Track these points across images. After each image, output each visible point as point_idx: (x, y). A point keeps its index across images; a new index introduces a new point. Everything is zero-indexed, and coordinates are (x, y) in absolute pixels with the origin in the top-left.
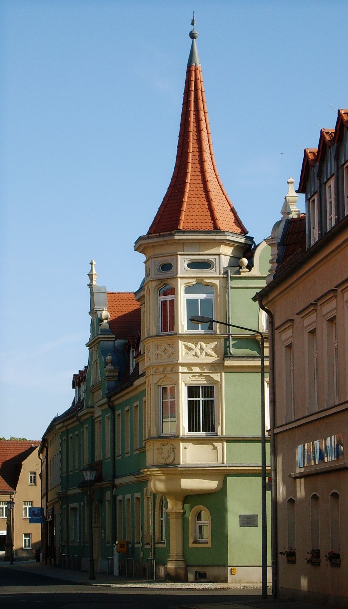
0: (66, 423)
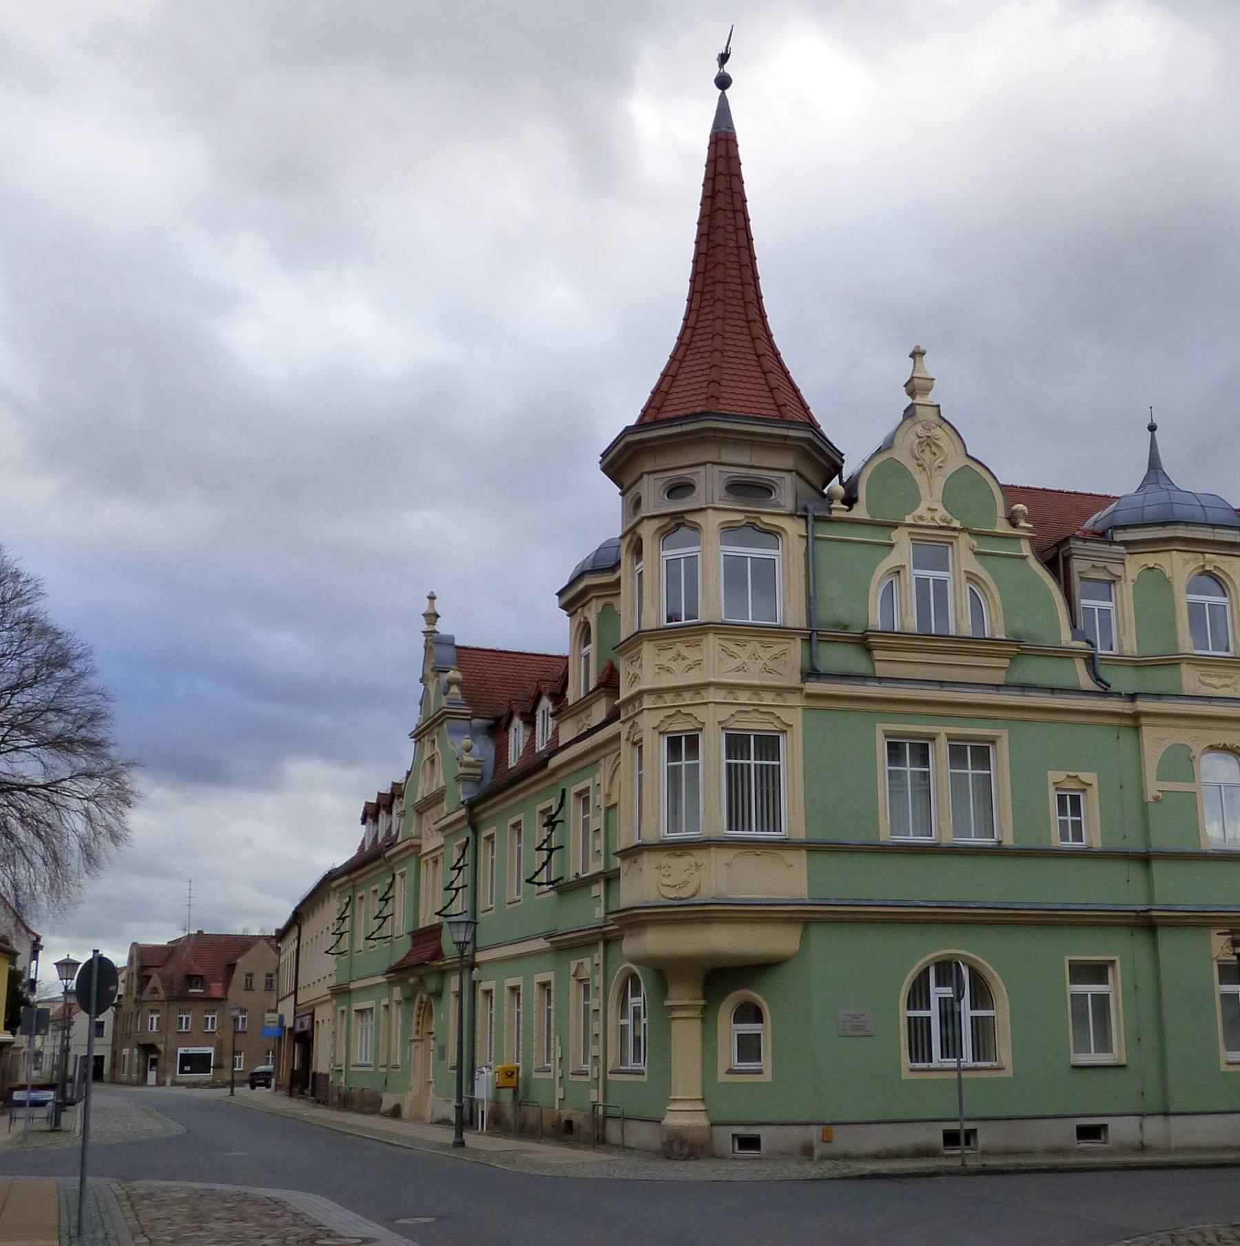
0: (353, 876)
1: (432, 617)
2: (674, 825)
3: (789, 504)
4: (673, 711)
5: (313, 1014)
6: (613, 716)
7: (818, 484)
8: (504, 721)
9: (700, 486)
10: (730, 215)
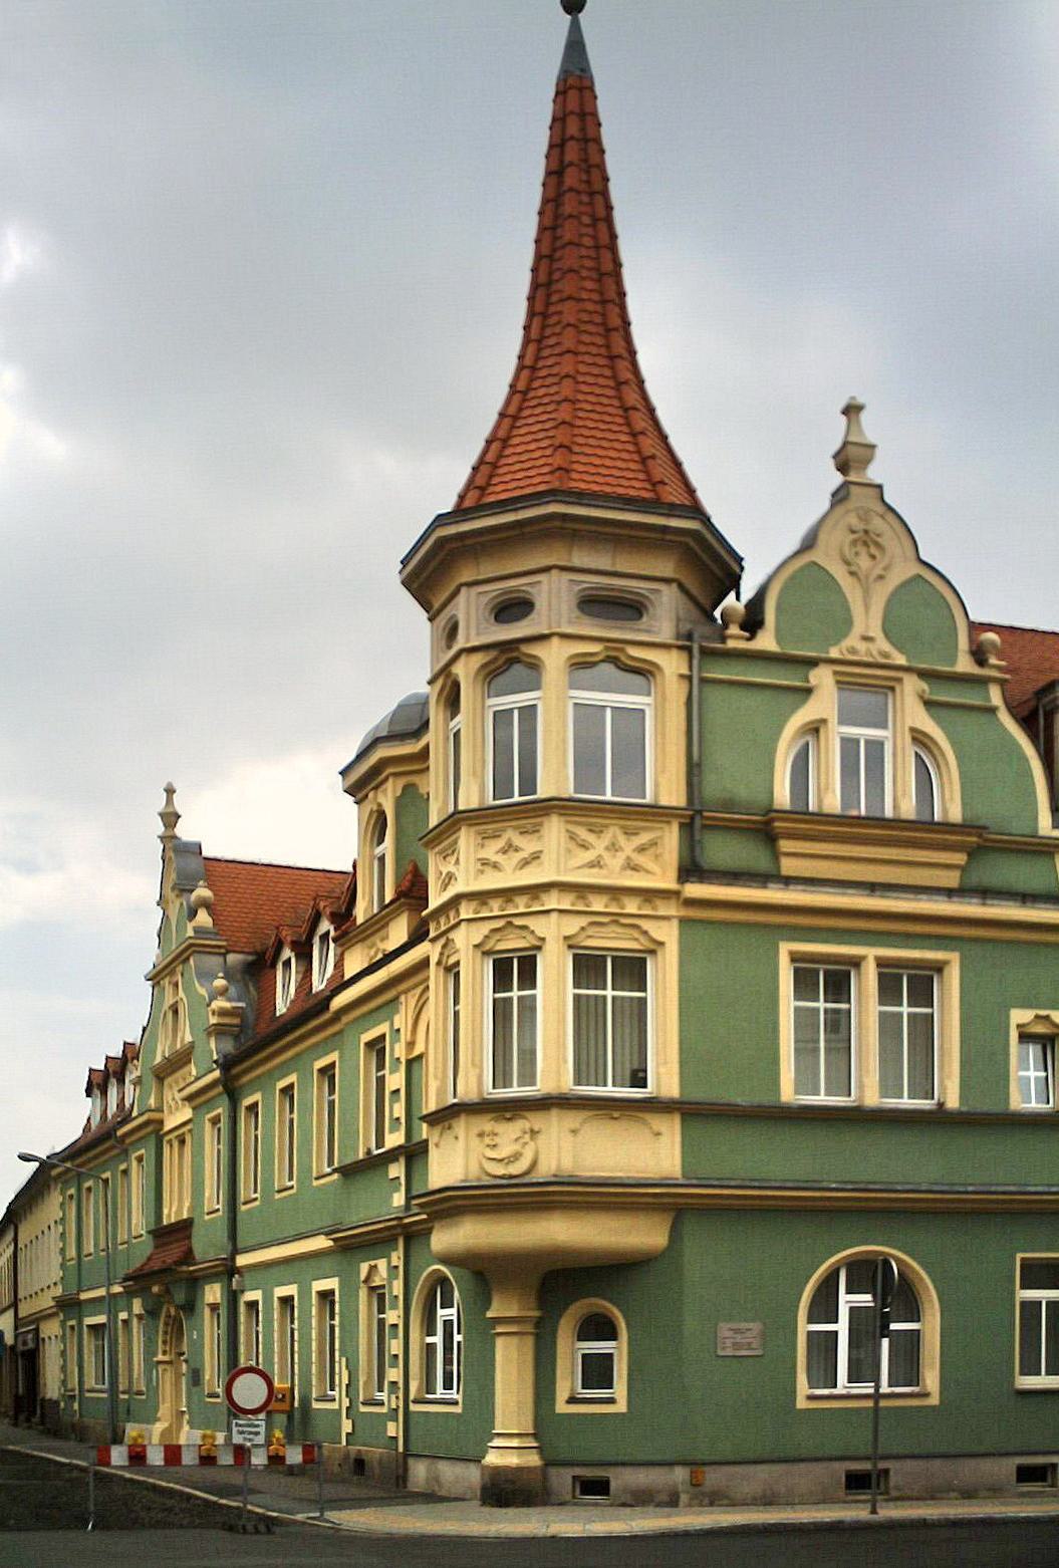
1: (170, 818)
2: (501, 1076)
3: (665, 632)
4: (500, 923)
5: (37, 1330)
6: (418, 936)
7: (708, 607)
8: (270, 953)
9: (541, 603)
10: (585, 198)
